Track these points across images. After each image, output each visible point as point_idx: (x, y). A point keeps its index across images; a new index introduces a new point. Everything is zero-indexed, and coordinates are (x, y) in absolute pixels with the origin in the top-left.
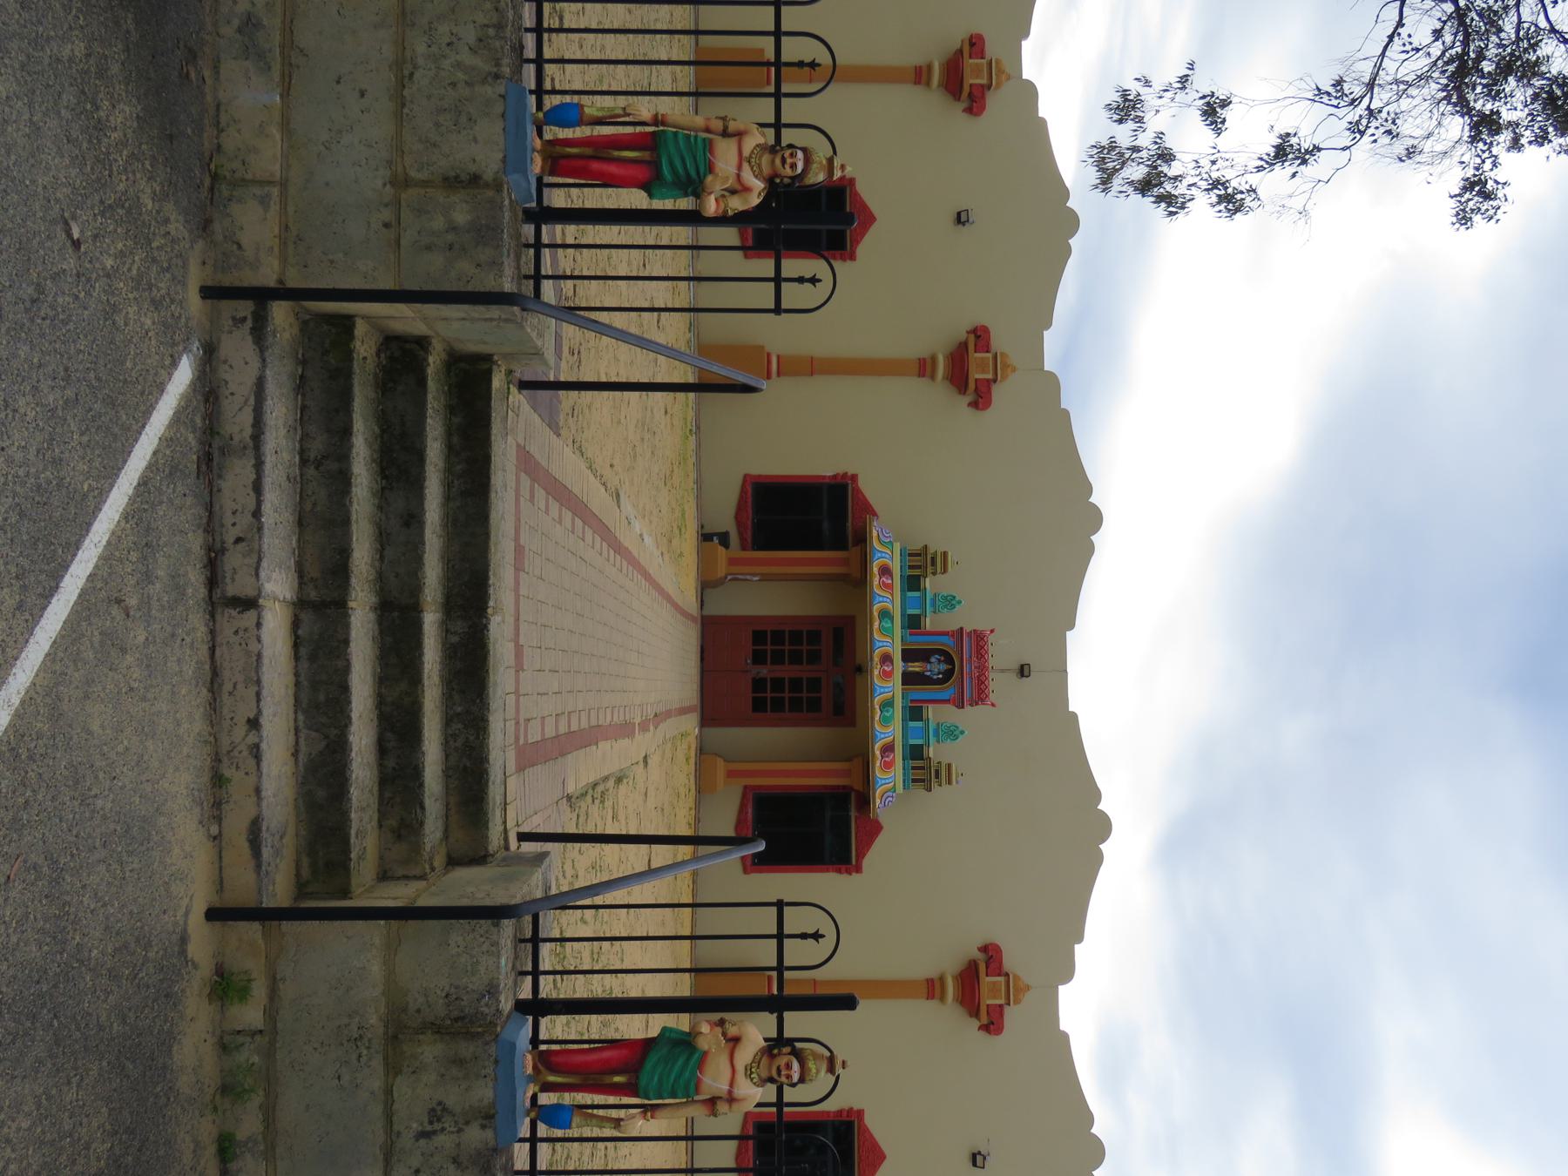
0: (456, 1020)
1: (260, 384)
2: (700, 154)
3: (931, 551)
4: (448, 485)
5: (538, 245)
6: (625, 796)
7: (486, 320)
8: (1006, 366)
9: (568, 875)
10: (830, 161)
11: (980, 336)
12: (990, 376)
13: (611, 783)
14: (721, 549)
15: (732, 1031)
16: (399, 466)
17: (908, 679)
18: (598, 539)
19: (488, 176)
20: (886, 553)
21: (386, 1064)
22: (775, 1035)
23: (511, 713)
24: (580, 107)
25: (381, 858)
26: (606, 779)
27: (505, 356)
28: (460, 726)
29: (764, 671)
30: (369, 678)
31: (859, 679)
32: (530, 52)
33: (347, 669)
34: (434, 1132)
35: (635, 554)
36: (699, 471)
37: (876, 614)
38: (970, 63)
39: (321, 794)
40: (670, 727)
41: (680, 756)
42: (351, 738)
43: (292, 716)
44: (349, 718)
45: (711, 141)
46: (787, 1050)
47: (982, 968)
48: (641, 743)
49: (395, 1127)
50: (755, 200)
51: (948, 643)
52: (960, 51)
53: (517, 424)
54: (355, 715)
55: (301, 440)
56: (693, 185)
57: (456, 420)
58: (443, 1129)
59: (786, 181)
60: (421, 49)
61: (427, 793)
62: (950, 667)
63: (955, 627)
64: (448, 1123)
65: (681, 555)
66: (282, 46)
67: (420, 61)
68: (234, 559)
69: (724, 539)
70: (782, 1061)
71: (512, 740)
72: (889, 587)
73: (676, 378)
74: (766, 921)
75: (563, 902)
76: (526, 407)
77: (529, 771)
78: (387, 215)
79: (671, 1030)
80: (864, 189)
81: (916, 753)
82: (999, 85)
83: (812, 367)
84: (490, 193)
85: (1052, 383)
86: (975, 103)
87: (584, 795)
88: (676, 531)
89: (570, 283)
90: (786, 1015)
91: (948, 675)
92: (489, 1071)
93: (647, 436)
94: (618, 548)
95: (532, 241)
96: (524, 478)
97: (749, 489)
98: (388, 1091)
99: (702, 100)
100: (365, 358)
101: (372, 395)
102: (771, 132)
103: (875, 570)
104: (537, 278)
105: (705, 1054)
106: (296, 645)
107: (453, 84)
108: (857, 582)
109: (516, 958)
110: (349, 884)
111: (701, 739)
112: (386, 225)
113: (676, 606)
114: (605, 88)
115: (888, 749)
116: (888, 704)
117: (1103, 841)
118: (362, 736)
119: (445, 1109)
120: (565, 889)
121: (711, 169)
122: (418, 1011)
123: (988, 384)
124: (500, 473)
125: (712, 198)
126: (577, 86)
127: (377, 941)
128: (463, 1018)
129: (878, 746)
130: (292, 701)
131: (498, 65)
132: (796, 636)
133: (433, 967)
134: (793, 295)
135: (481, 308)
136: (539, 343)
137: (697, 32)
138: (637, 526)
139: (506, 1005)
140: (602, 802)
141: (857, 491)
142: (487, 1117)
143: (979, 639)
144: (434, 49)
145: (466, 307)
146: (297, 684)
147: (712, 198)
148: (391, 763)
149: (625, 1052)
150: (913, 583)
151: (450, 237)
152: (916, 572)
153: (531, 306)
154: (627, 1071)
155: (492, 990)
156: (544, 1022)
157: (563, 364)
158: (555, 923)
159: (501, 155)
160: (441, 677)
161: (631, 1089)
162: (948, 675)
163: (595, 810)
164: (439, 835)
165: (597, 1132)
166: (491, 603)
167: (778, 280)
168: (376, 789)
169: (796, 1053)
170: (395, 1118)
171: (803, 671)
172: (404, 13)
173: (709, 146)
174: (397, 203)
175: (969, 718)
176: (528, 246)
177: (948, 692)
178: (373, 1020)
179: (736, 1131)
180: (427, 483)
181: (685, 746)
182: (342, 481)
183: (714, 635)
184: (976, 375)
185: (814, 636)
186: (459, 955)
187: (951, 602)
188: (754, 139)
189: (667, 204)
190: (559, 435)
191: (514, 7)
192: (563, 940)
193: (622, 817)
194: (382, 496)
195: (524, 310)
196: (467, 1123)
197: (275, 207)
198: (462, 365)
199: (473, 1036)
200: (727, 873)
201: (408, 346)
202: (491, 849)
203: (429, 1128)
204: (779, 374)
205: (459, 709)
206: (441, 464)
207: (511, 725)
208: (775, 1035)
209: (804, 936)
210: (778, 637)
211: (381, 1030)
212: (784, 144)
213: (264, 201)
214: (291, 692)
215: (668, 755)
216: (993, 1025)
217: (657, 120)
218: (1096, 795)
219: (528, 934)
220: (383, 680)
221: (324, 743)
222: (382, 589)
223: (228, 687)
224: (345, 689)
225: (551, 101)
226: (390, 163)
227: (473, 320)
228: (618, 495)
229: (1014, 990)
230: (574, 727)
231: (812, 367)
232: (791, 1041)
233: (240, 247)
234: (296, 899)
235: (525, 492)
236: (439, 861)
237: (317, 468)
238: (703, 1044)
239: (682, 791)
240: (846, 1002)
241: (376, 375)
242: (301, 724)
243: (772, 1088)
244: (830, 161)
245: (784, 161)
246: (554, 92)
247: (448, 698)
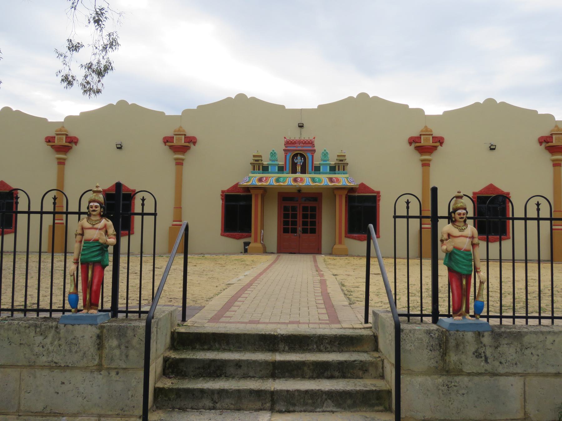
0: (440, 347)
2: (92, 245)
3: (252, 161)
4: (224, 350)
5: (127, 312)
6: (350, 283)
7: (157, 333)
8: (179, 131)
9: (381, 305)
10: (94, 192)
11: (167, 140)
12: (183, 137)
13: (344, 288)
14: (251, 245)
15: (445, 236)
16: (216, 370)
17: (303, 171)
18: (246, 292)
19: (98, 331)
20: (253, 179)
21: (458, 375)
22: (447, 220)
23: (317, 326)
24: (70, 293)
25: (375, 378)
26: (342, 290)
27: (172, 326)
28: (322, 346)
29: (299, 229)
30: (303, 382)
31: (303, 191)
32: (47, 315)
33: (298, 391)
34: (485, 356)
35: (252, 278)
36: (220, 254)
37: (277, 184)
38: (57, 143)
39: (349, 402)
40: (322, 266)
41: (332, 262)
42: (327, 389)
43: (318, 413)
44: (318, 390)
45: (85, 240)
46: (453, 215)
48: (328, 276)
49: (483, 371)
50: (110, 223)
51: (290, 156)
52: (52, 146)
53: (200, 322)
54: (317, 388)
55: (205, 409)
56: (103, 248)
57: (198, 347)
58: (484, 352)
59: (102, 210)
60: (44, 359)
61: (349, 359)
62: (299, 156)
63: (283, 152)
64: (481, 350)
65: (253, 261)
66: (42, 416)
67: (50, 359)
69: (247, 244)
70: (457, 217)
71: (328, 325)
73: (182, 262)
74: (402, 223)
75: (393, 303)
76: (193, 319)
77: (340, 319)
78: (113, 373)
79: (445, 261)
81: (333, 169)
82: (66, 131)
83: (178, 208)
84: (105, 331)
85: (187, 112)
86: (73, 141)
87: (349, 298)
88: (243, 263)
89: (142, 302)
90: (439, 215)
91: (302, 156)
92: (461, 334)
93: (205, 273)
94: (250, 285)
95: (125, 314)
96: (221, 320)
98: (469, 374)
99: (68, 251)
100: (172, 383)
101: (187, 380)
102: (82, 216)
103: (260, 184)
104: (140, 312)
105: (454, 247)
106: (289, 412)
107: (60, 345)
108: (264, 191)
109: (415, 323)
110: (385, 391)
111: (326, 254)
112: (117, 373)
114: (63, 287)
115: (331, 180)
116: (313, 180)
117: (368, 96)
118: (326, 385)
119: (476, 352)
120: (389, 306)
121: (97, 241)
122: (437, 362)
123: (186, 137)
124: (220, 329)
125: (109, 240)
126: (61, 298)
127: (409, 379)
128: (440, 344)
129: (330, 184)
130: (311, 413)
131: (52, 327)
132: (286, 216)
133: (419, 356)
134: (149, 208)
135: (152, 335)
136: (167, 312)
137: (40, 252)
138: (241, 277)
139: (434, 327)
140: (352, 292)
141: (228, 191)
142: (479, 335)
144: (45, 353)
145: (152, 341)
146: (305, 411)
147: (109, 240)
148: (337, 374)
149: (453, 280)
150: (265, 169)
151: (123, 347)
152: (261, 168)
153: (152, 315)
154: (461, 279)
155: (429, 332)
157: (175, 304)
158: (401, 307)
159: (90, 326)
160: (302, 353)
161: (468, 277)
162: (302, 156)
163: (355, 295)
164: (365, 355)
165: (485, 292)
166: (272, 333)
167: (143, 214)
168: (347, 380)
169: (455, 210)
170: (480, 372)
171: (300, 213)
172: (30, 366)
173: (87, 241)
174: (109, 369)
175: (319, 148)
176: (127, 316)
177: (309, 156)
178: (440, 380)
179: (485, 243)
180: (223, 358)
181: (329, 260)
182: (222, 393)
183: (285, 248)
184: (182, 143)
185: (286, 209)
186: (414, 346)
187: (273, 154)
188: (85, 222)
189: (111, 258)
190: (204, 307)
191: (28, 320)
192: (408, 307)
193: (357, 284)
194: (228, 376)
195: (153, 318)
196: (481, 343)
198: (175, 344)
199: (447, 341)
200: (382, 242)
201: (167, 366)
202: (372, 334)
203: (483, 358)
204: (181, 221)
205: (315, 346)
206: (216, 353)
207: (321, 326)
208: (447, 220)
209: (408, 208)
210: (286, 223)
211: (445, 377)
212: (87, 211)
214: (307, 414)
215: (333, 267)
216: (440, 141)
217: (77, 263)
218: (351, 98)
219: (406, 318)
220: (303, 377)
221: (329, 401)
222: (266, 377)
224: (307, 392)
225: (68, 306)
226: (91, 372)
227: (157, 339)
228: (229, 284)
229: (427, 132)
230: (322, 302)
231: (178, 208)
232: (450, 213)
234: (392, 412)
235: (227, 320)
236: (376, 354)
237: (217, 403)
238: (450, 248)
239: (347, 261)
240: (434, 191)
241: (179, 379)
242: (321, 410)
244: (94, 192)
245: (94, 211)
246: (64, 306)
247: (310, 351)
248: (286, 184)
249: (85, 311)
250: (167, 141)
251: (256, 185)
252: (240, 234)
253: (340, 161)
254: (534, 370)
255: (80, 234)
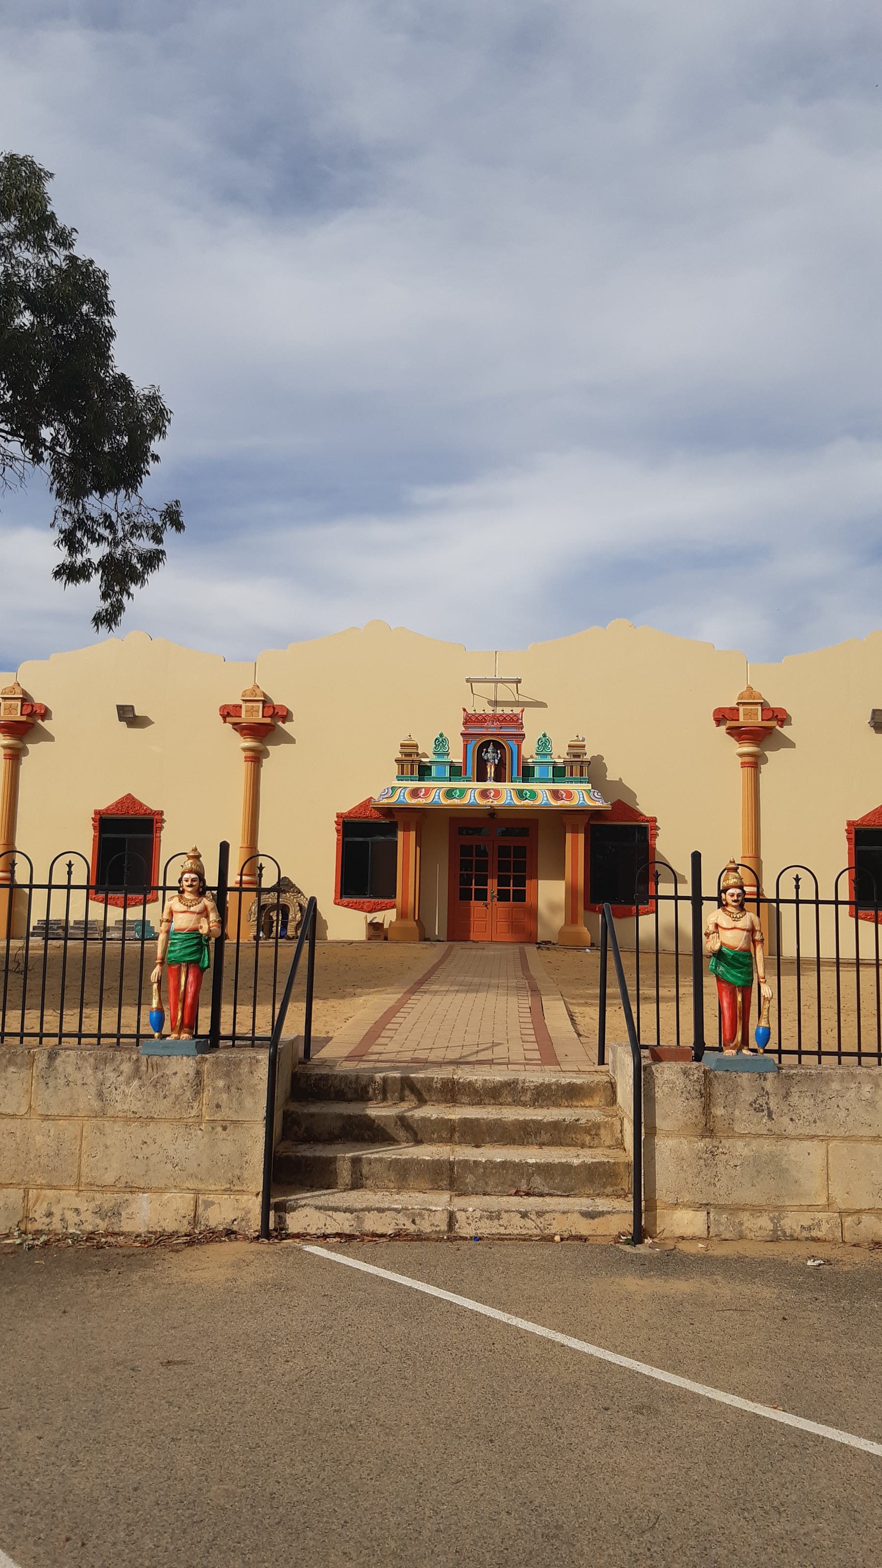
1: (317, 1208)
3: (399, 756)
15: (712, 928)
17: (499, 778)
34: (768, 1109)
46: (723, 895)
47: (730, 724)
51: (474, 744)
58: (767, 1103)
63: (461, 738)
66: (113, 1192)
68: (425, 1227)
72: (428, 790)
80: (106, 801)
91: (498, 746)
97: (346, 900)
113: (441, 962)
115: (556, 794)
122: (696, 1117)
129: (554, 803)
132: (465, 865)
143: (469, 720)
149: (724, 994)
150: (424, 771)
151: (233, 1090)
152: (416, 768)
156: (708, 1044)
159: (185, 1058)
162: (498, 746)
169: (725, 891)
175: (533, 726)
179: (874, 924)
185: (465, 850)
190: (331, 1038)
196: (763, 1089)
197: (212, 1198)
203: (766, 1112)
213: (208, 1204)
223: (502, 1230)
232: (720, 894)
233: (235, 1220)
243: (747, 905)
248: (466, 801)
249: (174, 1035)
250: (229, 715)
251: (408, 804)
252: (373, 900)
253: (575, 756)
254: (842, 1132)
255: (167, 921)
